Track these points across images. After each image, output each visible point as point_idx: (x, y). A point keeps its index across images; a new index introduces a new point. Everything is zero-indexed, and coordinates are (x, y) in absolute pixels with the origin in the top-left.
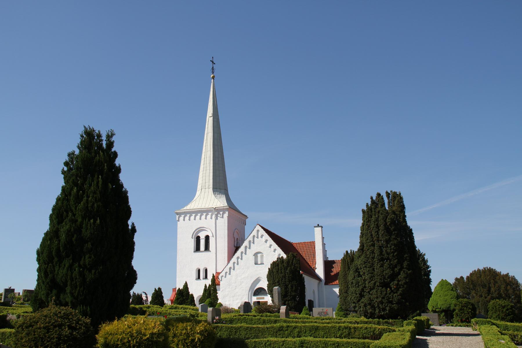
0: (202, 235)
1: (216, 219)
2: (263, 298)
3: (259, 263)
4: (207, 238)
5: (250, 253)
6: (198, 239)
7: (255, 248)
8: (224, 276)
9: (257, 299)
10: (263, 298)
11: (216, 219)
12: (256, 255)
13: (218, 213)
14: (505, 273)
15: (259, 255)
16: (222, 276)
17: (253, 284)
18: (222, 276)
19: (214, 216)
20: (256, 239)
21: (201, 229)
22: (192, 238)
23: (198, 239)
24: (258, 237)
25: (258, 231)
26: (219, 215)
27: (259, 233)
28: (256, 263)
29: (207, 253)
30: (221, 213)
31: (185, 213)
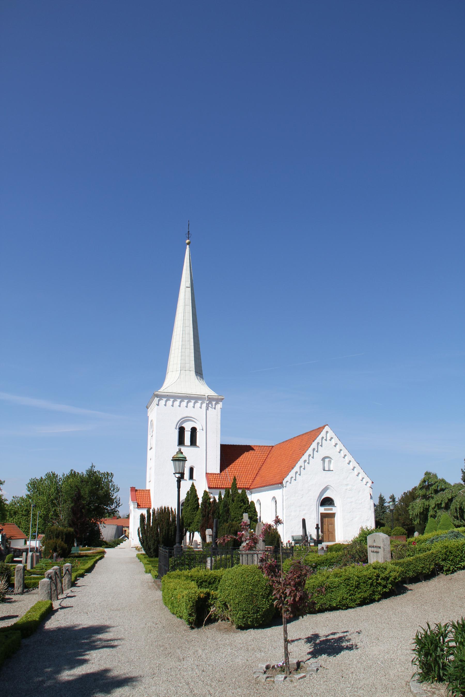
0: (188, 427)
1: (207, 409)
2: (332, 510)
3: (326, 469)
4: (194, 430)
5: (318, 456)
6: (182, 431)
7: (323, 452)
8: (289, 481)
9: (325, 510)
10: (332, 510)
11: (207, 409)
12: (323, 459)
13: (210, 403)
14: (67, 472)
15: (327, 460)
16: (287, 482)
17: (321, 493)
18: (287, 482)
19: (204, 405)
20: (324, 441)
21: (187, 419)
22: (176, 428)
23: (182, 431)
24: (326, 440)
25: (327, 432)
26: (210, 405)
27: (328, 435)
28: (324, 470)
29: (193, 449)
30: (214, 403)
31: (160, 397)
